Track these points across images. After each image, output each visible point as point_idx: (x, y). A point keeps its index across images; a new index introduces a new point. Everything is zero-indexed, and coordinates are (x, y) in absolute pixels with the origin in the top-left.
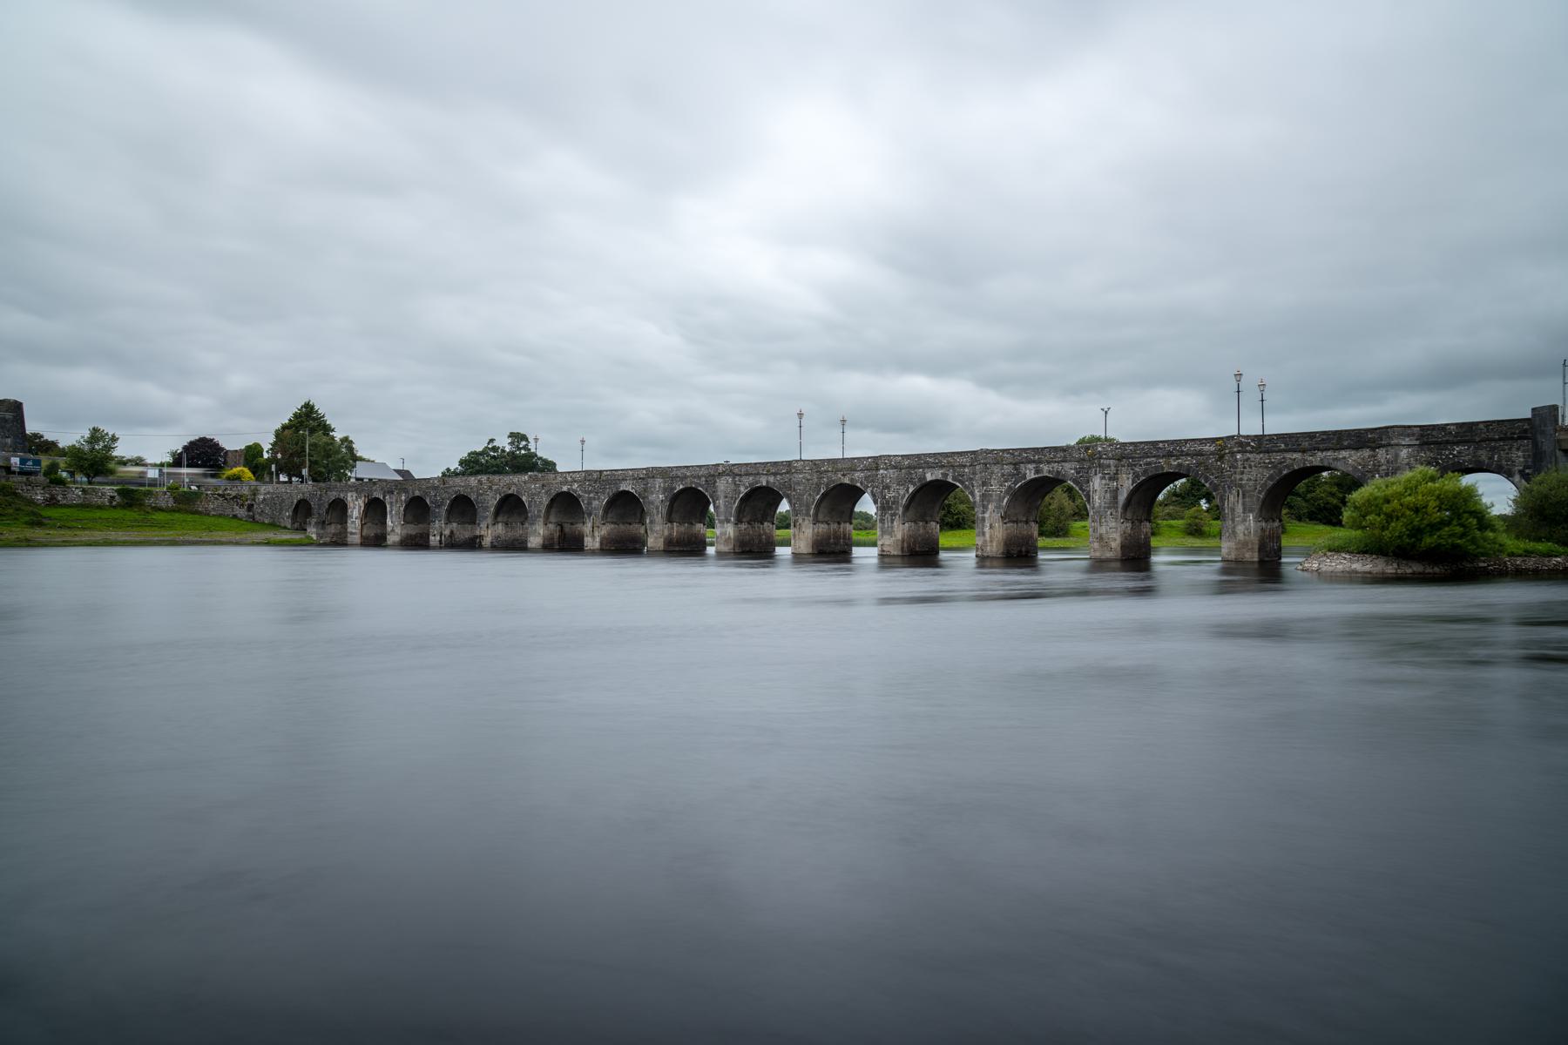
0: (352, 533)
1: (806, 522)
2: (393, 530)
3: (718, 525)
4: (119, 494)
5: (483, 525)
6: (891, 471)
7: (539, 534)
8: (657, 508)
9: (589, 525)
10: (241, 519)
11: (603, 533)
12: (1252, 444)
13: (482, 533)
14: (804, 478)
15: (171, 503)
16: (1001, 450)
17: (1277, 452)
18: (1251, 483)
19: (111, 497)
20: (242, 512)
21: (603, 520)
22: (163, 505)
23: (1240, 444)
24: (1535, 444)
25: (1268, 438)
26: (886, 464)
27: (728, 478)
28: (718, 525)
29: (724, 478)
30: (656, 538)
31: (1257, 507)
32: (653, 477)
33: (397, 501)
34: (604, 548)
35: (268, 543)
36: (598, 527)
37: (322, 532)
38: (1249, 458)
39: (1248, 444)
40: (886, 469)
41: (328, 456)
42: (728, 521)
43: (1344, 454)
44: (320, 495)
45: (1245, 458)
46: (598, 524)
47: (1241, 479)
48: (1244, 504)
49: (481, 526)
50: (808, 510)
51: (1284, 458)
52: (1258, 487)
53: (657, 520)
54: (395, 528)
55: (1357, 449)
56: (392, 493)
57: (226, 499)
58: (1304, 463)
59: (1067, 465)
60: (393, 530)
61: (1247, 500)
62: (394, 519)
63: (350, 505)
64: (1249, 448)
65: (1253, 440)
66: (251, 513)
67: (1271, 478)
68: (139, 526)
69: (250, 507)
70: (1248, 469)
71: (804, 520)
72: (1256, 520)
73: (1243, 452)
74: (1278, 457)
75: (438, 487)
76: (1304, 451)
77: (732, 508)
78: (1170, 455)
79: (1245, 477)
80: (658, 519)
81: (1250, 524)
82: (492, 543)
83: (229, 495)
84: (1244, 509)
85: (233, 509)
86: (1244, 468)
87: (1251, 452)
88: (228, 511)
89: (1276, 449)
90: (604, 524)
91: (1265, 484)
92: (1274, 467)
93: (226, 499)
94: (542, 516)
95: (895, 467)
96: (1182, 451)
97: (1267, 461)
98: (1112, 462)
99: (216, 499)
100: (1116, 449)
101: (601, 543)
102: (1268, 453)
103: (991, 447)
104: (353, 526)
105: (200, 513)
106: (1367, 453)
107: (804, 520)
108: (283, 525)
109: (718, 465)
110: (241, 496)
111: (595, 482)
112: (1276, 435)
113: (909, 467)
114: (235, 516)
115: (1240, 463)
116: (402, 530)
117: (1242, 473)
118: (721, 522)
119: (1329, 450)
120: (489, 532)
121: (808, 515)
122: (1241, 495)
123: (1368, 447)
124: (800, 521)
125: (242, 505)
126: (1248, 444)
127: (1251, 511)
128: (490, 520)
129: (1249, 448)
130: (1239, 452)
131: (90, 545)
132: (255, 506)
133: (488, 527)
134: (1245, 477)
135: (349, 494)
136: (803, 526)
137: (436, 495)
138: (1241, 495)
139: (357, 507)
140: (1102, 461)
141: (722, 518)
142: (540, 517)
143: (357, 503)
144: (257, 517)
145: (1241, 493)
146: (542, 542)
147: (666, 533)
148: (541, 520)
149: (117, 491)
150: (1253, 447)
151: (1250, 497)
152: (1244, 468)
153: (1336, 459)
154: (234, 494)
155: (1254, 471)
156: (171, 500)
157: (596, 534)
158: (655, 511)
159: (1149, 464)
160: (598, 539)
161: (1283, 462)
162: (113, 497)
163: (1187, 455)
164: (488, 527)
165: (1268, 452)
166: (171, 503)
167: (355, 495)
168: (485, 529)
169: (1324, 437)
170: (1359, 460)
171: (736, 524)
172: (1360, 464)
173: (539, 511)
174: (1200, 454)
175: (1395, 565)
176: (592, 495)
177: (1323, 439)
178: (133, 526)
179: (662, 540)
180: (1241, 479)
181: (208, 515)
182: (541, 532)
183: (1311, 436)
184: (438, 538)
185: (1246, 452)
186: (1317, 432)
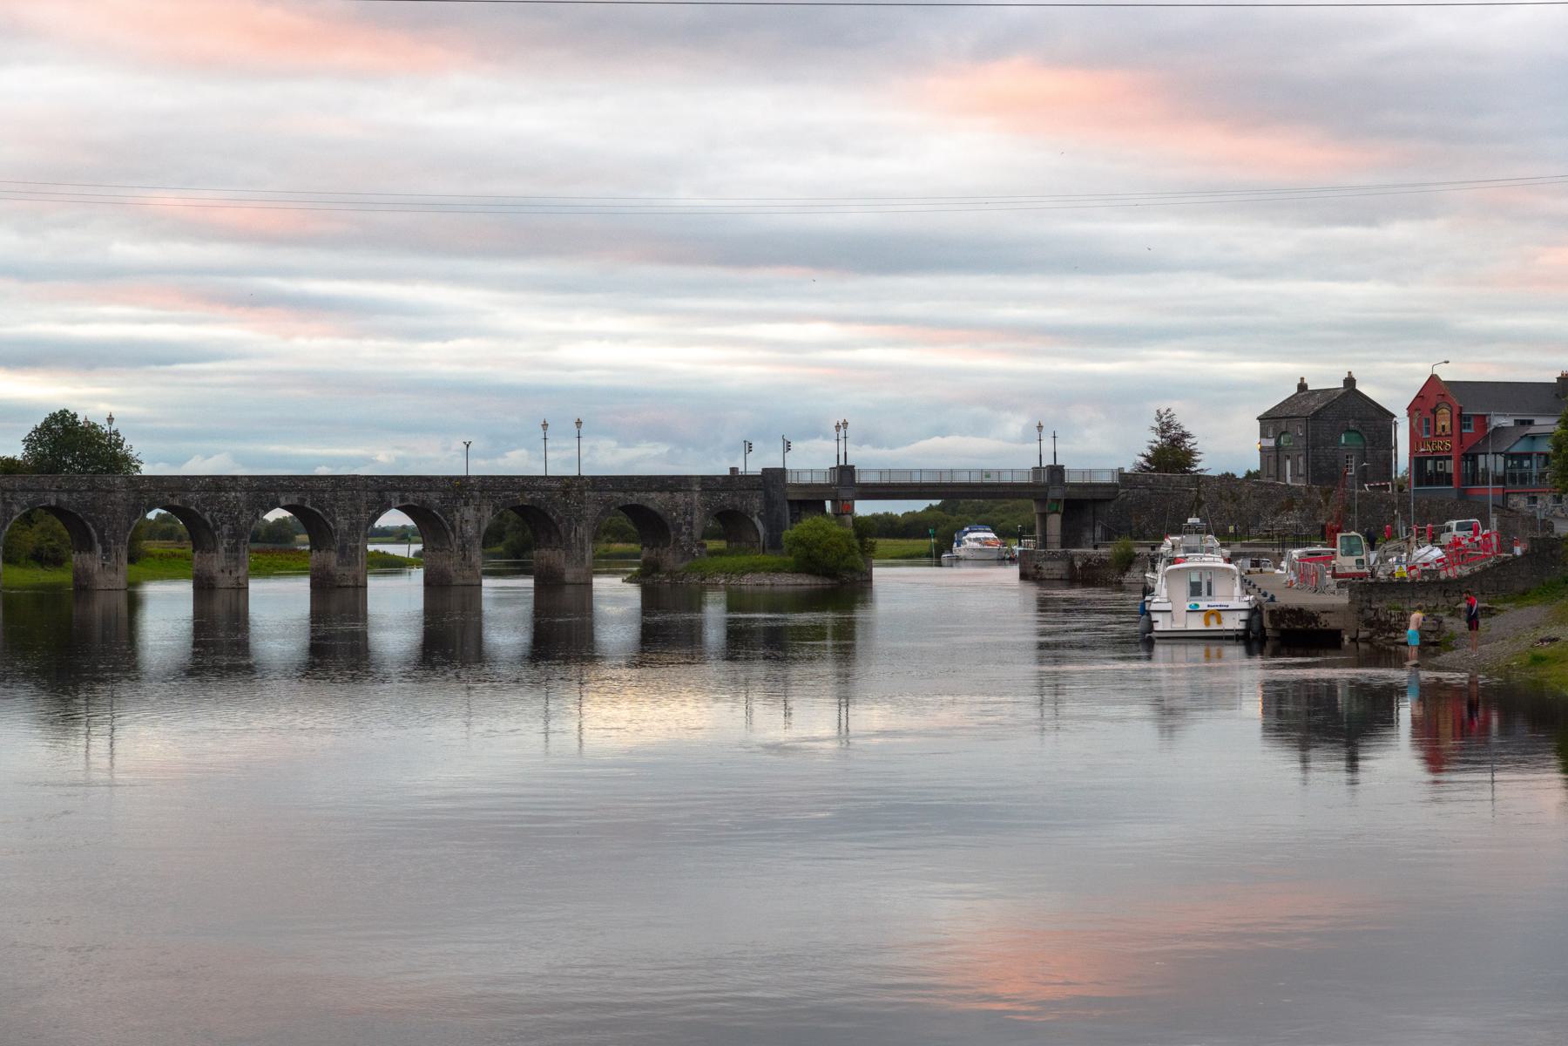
24: (767, 495)
43: (653, 495)
59: (432, 495)
74: (607, 495)
76: (625, 492)
78: (524, 489)
106: (667, 495)
172: (663, 504)
174: (548, 489)
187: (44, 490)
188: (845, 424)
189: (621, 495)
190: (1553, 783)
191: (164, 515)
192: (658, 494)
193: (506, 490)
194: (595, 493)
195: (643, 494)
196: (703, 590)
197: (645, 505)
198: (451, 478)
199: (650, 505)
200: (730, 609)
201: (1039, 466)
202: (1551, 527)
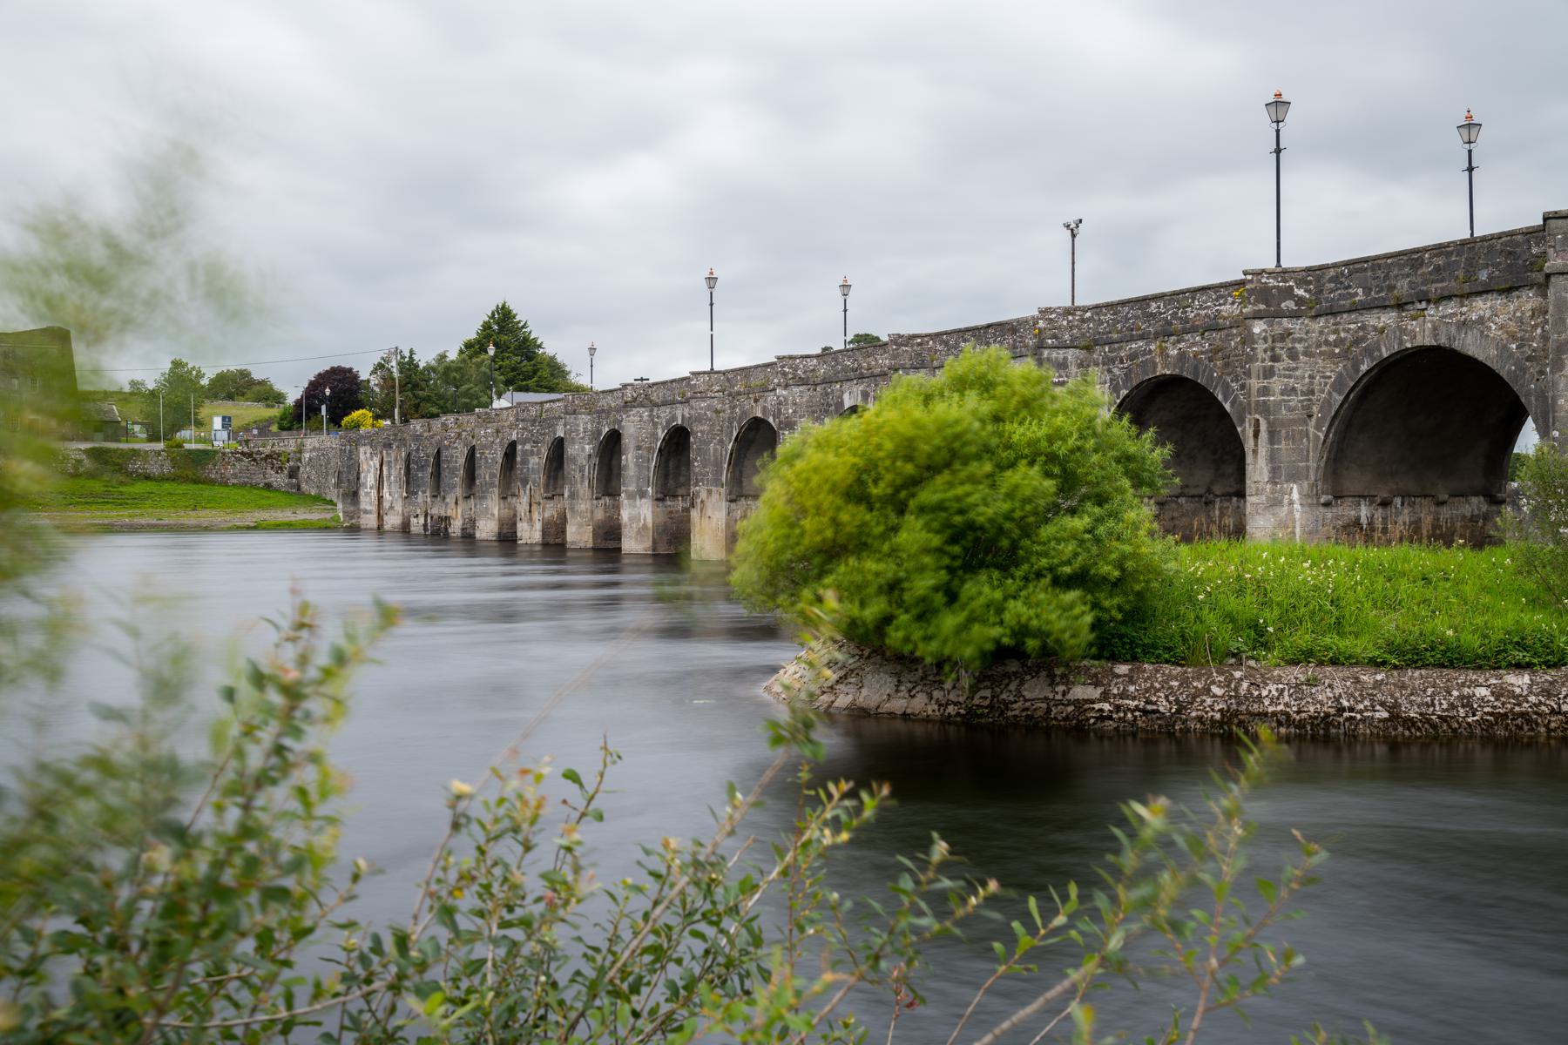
0: (366, 512)
1: (715, 497)
2: (391, 508)
3: (626, 502)
4: (88, 456)
5: (450, 499)
6: (796, 390)
7: (493, 515)
8: (582, 470)
9: (525, 500)
10: (277, 490)
11: (547, 515)
12: (1301, 292)
13: (449, 513)
14: (709, 408)
15: (167, 469)
16: (930, 336)
17: (1349, 311)
18: (1295, 400)
19: (77, 461)
20: (279, 480)
21: (547, 490)
22: (156, 471)
23: (1264, 294)
25: (1332, 272)
26: (784, 374)
27: (643, 409)
28: (626, 502)
29: (635, 411)
30: (581, 526)
31: (1314, 463)
32: (574, 412)
33: (396, 460)
34: (552, 541)
35: (289, 527)
36: (539, 504)
37: (352, 508)
38: (1288, 333)
39: (1288, 293)
40: (786, 386)
41: (875, 398)
42: (643, 495)
43: (1481, 307)
44: (350, 451)
45: (1278, 330)
46: (537, 498)
47: (1265, 391)
48: (1273, 458)
49: (448, 500)
50: (718, 473)
51: (1363, 328)
52: (1315, 409)
53: (581, 492)
54: (394, 505)
55: (1508, 291)
56: (389, 446)
57: (254, 460)
58: (1401, 342)
60: (391, 508)
61: (1283, 446)
62: (393, 489)
63: (364, 467)
64: (1289, 304)
65: (1302, 283)
66: (294, 480)
67: (1338, 385)
68: (87, 503)
69: (293, 473)
70: (1287, 363)
71: (710, 492)
72: (1312, 501)
73: (1272, 315)
74: (1350, 325)
75: (421, 435)
76: (1400, 306)
77: (649, 469)
79: (1277, 384)
80: (584, 489)
81: (1291, 512)
82: (463, 529)
83: (259, 453)
84: (1275, 471)
85: (265, 474)
86: (1275, 358)
87: (1294, 315)
88: (258, 478)
89: (1346, 303)
90: (552, 498)
91: (1328, 402)
92: (1345, 355)
93: (254, 460)
94: (497, 483)
95: (802, 382)
96: (1187, 320)
97: (1332, 338)
98: (1071, 354)
99: (239, 460)
100: (1083, 321)
101: (544, 533)
102: (1334, 314)
103: (906, 330)
104: (368, 499)
105: (212, 482)
107: (710, 492)
108: (328, 499)
109: (625, 386)
110: (279, 455)
111: (534, 422)
112: (1347, 264)
113: (827, 381)
114: (268, 486)
115: (1260, 346)
116: (404, 506)
117: (1269, 373)
118: (631, 496)
119: (1450, 298)
120: (459, 511)
121: (717, 482)
122: (1263, 435)
123: (1531, 286)
124: (703, 495)
125: (281, 468)
126: (1288, 293)
127: (1294, 477)
128: (459, 491)
129: (1289, 304)
130: (1258, 316)
131: (269, 529)
132: (302, 469)
133: (456, 503)
134: (1277, 384)
135: (362, 450)
136: (708, 504)
137: (418, 449)
138: (1263, 435)
139: (372, 470)
140: (1046, 353)
141: (632, 488)
142: (492, 485)
143: (371, 463)
144: (304, 486)
145: (1263, 427)
146: (496, 529)
147: (600, 515)
148: (496, 490)
149: (86, 451)
150: (1300, 301)
151: (1291, 437)
152: (1275, 358)
153: (1464, 325)
154: (267, 450)
155: (1304, 368)
156: (168, 463)
157: (536, 516)
158: (578, 476)
159: (1133, 356)
160: (538, 526)
161: (1363, 339)
162: (79, 462)
163: (1194, 330)
164: (456, 503)
165: (1332, 313)
166: (167, 469)
167: (369, 450)
168: (453, 506)
169: (1440, 261)
170: (1513, 326)
171: (504, 498)
172: (1513, 337)
173: (492, 476)
174: (1213, 326)
175: (889, 688)
176: (528, 447)
177: (1438, 269)
178: (78, 503)
179: (590, 528)
180: (1265, 391)
181: (226, 484)
182: (496, 512)
183: (1411, 259)
184: (422, 520)
185: (1281, 314)
186: (1425, 249)
187: (858, 349)
188: (1081, 221)
189: (1387, 319)
190: (587, 554)
191: (1054, 888)
192: (1499, 302)
193: (1132, 339)
194: (1322, 322)
195: (1450, 308)
196: (1084, 589)
197: (1456, 346)
198: (1440, 249)
199: (1471, 345)
200: (620, 549)
201: (1068, 304)
202: (182, 447)
